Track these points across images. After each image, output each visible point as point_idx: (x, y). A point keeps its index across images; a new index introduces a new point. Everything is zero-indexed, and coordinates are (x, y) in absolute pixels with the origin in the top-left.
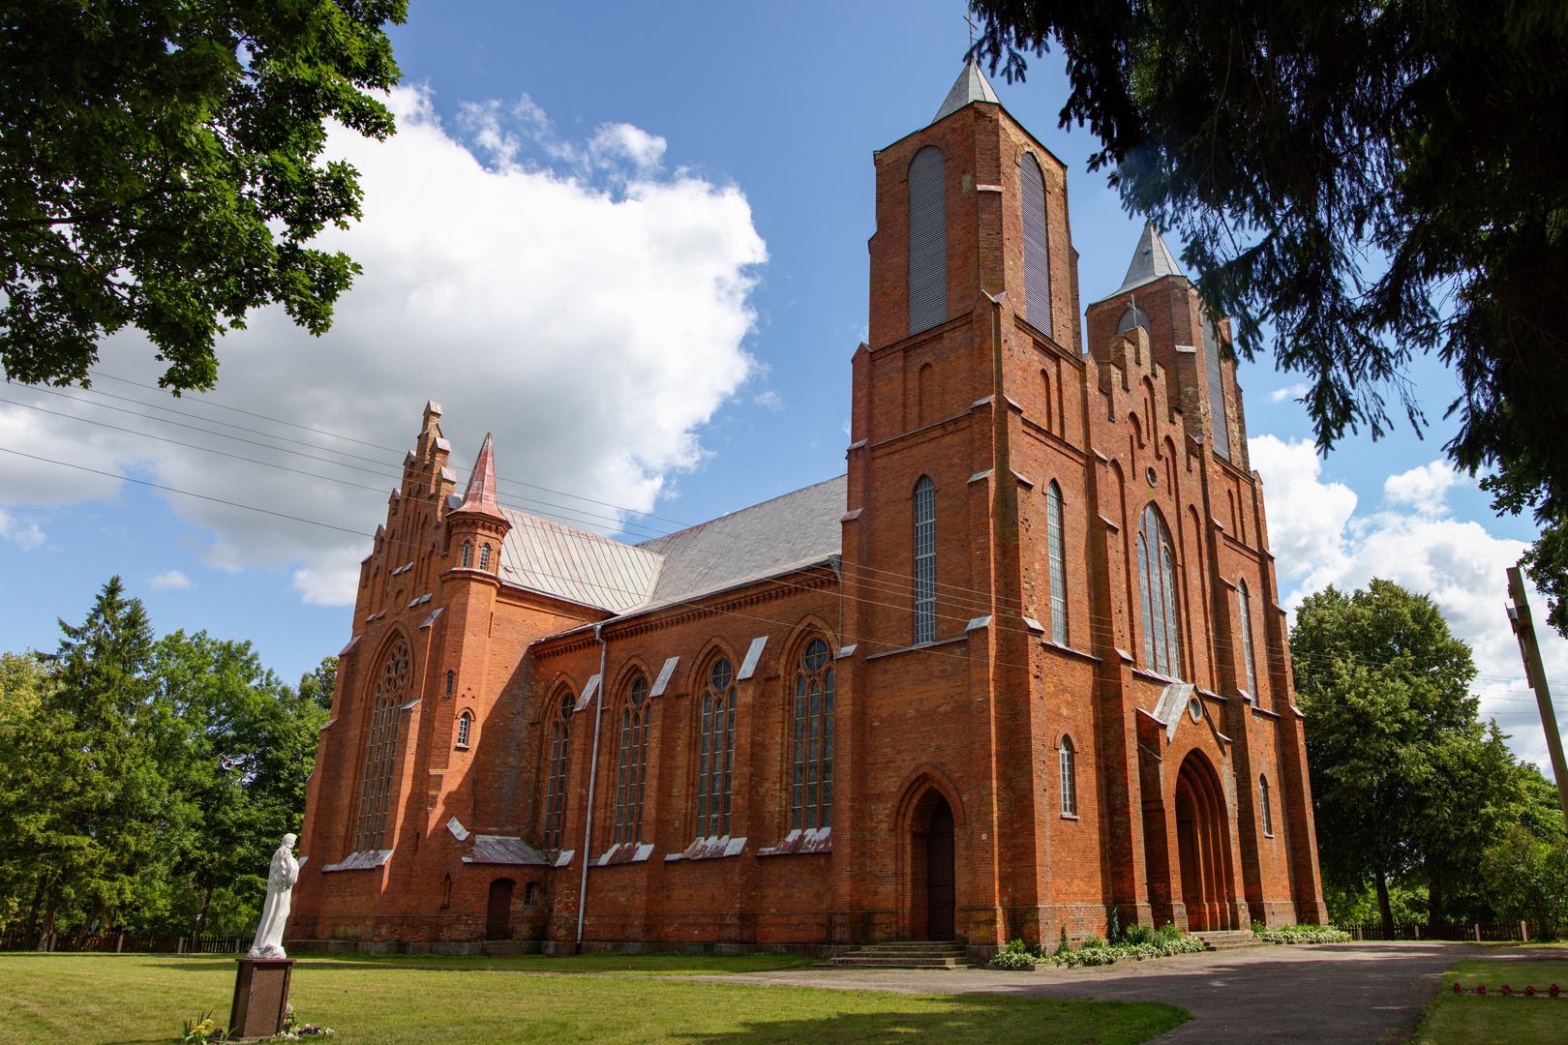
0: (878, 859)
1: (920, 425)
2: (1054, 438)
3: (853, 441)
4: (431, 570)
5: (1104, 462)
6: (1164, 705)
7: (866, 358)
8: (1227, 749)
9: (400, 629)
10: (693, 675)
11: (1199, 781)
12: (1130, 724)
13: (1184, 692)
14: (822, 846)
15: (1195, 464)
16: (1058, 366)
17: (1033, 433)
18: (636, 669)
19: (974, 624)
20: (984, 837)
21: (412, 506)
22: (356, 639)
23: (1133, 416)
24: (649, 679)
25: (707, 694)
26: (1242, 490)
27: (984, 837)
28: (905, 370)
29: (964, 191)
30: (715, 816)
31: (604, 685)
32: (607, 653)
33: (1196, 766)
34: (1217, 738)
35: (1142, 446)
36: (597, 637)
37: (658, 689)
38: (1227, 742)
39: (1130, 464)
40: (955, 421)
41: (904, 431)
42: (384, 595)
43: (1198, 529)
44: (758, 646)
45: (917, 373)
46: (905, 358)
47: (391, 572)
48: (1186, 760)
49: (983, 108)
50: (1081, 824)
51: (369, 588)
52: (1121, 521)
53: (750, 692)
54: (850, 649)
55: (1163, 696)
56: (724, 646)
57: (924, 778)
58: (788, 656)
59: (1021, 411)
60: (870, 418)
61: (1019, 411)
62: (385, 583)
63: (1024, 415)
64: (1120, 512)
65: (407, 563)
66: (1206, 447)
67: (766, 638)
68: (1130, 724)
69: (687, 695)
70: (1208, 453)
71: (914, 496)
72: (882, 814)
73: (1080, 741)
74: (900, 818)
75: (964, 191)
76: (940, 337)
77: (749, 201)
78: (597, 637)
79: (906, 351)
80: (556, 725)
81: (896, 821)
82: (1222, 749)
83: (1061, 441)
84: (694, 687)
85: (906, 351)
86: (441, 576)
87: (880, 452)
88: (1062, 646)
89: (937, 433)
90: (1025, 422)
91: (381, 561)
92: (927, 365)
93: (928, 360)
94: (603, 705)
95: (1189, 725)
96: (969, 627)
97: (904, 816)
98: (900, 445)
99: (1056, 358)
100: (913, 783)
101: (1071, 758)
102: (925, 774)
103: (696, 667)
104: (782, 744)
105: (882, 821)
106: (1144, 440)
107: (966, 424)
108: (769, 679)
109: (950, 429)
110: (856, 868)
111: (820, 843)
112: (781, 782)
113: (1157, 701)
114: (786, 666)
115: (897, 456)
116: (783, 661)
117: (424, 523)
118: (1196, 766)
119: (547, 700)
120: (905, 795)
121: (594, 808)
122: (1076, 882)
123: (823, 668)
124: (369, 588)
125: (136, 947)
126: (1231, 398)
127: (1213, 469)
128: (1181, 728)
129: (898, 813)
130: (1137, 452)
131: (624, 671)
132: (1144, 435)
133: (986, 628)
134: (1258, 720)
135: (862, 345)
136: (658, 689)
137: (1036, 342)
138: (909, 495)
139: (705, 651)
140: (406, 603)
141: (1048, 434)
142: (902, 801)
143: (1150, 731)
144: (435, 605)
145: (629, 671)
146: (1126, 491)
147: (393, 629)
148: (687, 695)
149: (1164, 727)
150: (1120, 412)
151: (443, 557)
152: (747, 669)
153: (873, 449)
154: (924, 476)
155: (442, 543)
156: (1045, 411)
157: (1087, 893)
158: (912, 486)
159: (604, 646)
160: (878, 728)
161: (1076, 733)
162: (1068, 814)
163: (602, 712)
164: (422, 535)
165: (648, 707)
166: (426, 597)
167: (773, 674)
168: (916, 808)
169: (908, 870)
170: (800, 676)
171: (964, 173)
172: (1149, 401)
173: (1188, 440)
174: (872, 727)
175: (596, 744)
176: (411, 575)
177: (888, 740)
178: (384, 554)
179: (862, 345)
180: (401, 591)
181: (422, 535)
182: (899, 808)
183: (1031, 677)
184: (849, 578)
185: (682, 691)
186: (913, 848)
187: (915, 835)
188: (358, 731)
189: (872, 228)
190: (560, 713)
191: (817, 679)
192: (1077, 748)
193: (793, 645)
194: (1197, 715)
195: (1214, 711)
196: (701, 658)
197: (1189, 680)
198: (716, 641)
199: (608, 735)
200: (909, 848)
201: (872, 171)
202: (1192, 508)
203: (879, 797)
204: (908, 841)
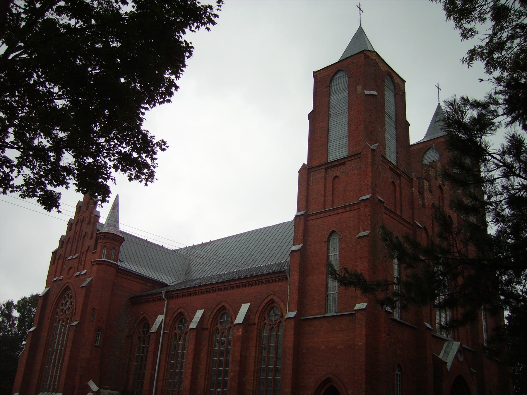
1: (324, 208)
2: (398, 216)
3: (297, 212)
4: (87, 259)
7: (306, 171)
9: (70, 286)
10: (211, 319)
16: (400, 180)
17: (388, 213)
18: (181, 314)
21: (79, 227)
22: (48, 289)
24: (188, 319)
25: (217, 329)
28: (325, 178)
29: (358, 93)
30: (219, 390)
31: (165, 320)
32: (167, 305)
36: (163, 297)
37: (193, 325)
40: (351, 206)
41: (332, 207)
42: (62, 268)
44: (245, 308)
45: (332, 180)
46: (326, 173)
47: (66, 258)
49: (368, 54)
51: (55, 265)
53: (241, 330)
54: (292, 314)
56: (227, 306)
57: (329, 380)
58: (260, 314)
59: (383, 203)
60: (307, 201)
62: (63, 263)
63: (385, 205)
65: (75, 254)
67: (250, 303)
69: (208, 329)
71: (328, 241)
75: (358, 93)
76: (344, 163)
77: (314, 79)
78: (163, 297)
79: (326, 169)
80: (139, 338)
83: (400, 217)
84: (211, 325)
85: (326, 169)
86: (92, 262)
87: (312, 218)
89: (341, 211)
90: (385, 208)
91: (62, 251)
92: (336, 177)
93: (337, 174)
94: (164, 331)
96: (355, 308)
98: (321, 215)
99: (399, 176)
102: (329, 378)
103: (212, 315)
104: (255, 357)
107: (356, 207)
108: (250, 325)
109: (348, 209)
112: (254, 376)
114: (259, 319)
115: (320, 220)
116: (257, 316)
117: (84, 236)
119: (136, 325)
121: (157, 380)
124: (55, 265)
128: (453, 364)
131: (176, 314)
135: (304, 164)
136: (193, 325)
137: (390, 168)
138: (326, 240)
139: (217, 308)
140: (73, 274)
141: (395, 214)
144: (88, 276)
145: (178, 315)
147: (66, 285)
148: (208, 329)
151: (93, 253)
152: (240, 319)
153: (308, 216)
154: (333, 231)
155: (93, 247)
158: (327, 235)
159: (166, 301)
163: (164, 333)
164: (83, 242)
165: (187, 332)
166: (84, 272)
167: (252, 322)
170: (265, 324)
171: (358, 84)
175: (160, 349)
176: (77, 260)
178: (64, 249)
179: (304, 164)
180: (71, 268)
181: (83, 242)
184: (294, 278)
185: (205, 326)
188: (46, 334)
190: (141, 332)
191: (274, 326)
193: (263, 308)
196: (215, 311)
198: (223, 304)
199: (166, 345)
201: (312, 80)
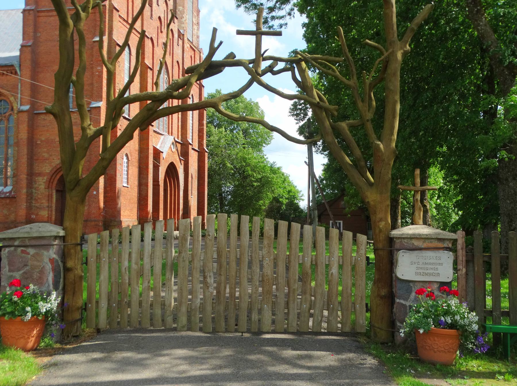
0: (39, 201)
5: (148, 38)
6: (162, 144)
8: (182, 162)
11: (171, 174)
12: (151, 151)
13: (170, 139)
14: (8, 194)
15: (181, 42)
19: (94, 105)
20: (95, 193)
23: (160, 18)
26: (196, 56)
27: (95, 193)
33: (172, 169)
34: (180, 159)
35: (162, 32)
38: (183, 160)
39: (156, 40)
43: (179, 71)
48: (168, 167)
50: (129, 189)
52: (152, 65)
55: (161, 141)
61: (118, 11)
64: (151, 61)
66: (185, 36)
68: (151, 151)
70: (185, 39)
72: (41, 183)
73: (131, 156)
74: (51, 184)
81: (49, 185)
82: (181, 162)
87: (43, 14)
88: (127, 117)
90: (120, 16)
95: (171, 152)
97: (52, 183)
100: (58, 169)
101: (128, 163)
105: (41, 185)
106: (163, 30)
110: (28, 204)
111: (7, 193)
113: (159, 142)
118: (172, 169)
120: (53, 174)
122: (127, 211)
123: (7, 114)
125: (146, 198)
126: (195, 14)
127: (187, 45)
128: (168, 154)
129: (50, 182)
130: (160, 34)
132: (163, 27)
133: (100, 107)
134: (193, 151)
142: (52, 176)
143: (157, 153)
146: (155, 52)
149: (162, 152)
150: (155, 16)
153: (38, 11)
156: (126, 11)
157: (130, 216)
160: (40, 144)
161: (130, 153)
162: (125, 185)
168: (58, 180)
169: (54, 206)
172: (166, 11)
173: (179, 31)
174: (37, 144)
177: (45, 150)
182: (50, 179)
183: (118, 129)
186: (56, 197)
187: (57, 191)
189: (247, 73)
191: (4, 119)
192: (130, 159)
194: (174, 148)
195: (179, 146)
197: (170, 134)
200: (54, 196)
202: (178, 62)
203: (40, 174)
204: (54, 194)
